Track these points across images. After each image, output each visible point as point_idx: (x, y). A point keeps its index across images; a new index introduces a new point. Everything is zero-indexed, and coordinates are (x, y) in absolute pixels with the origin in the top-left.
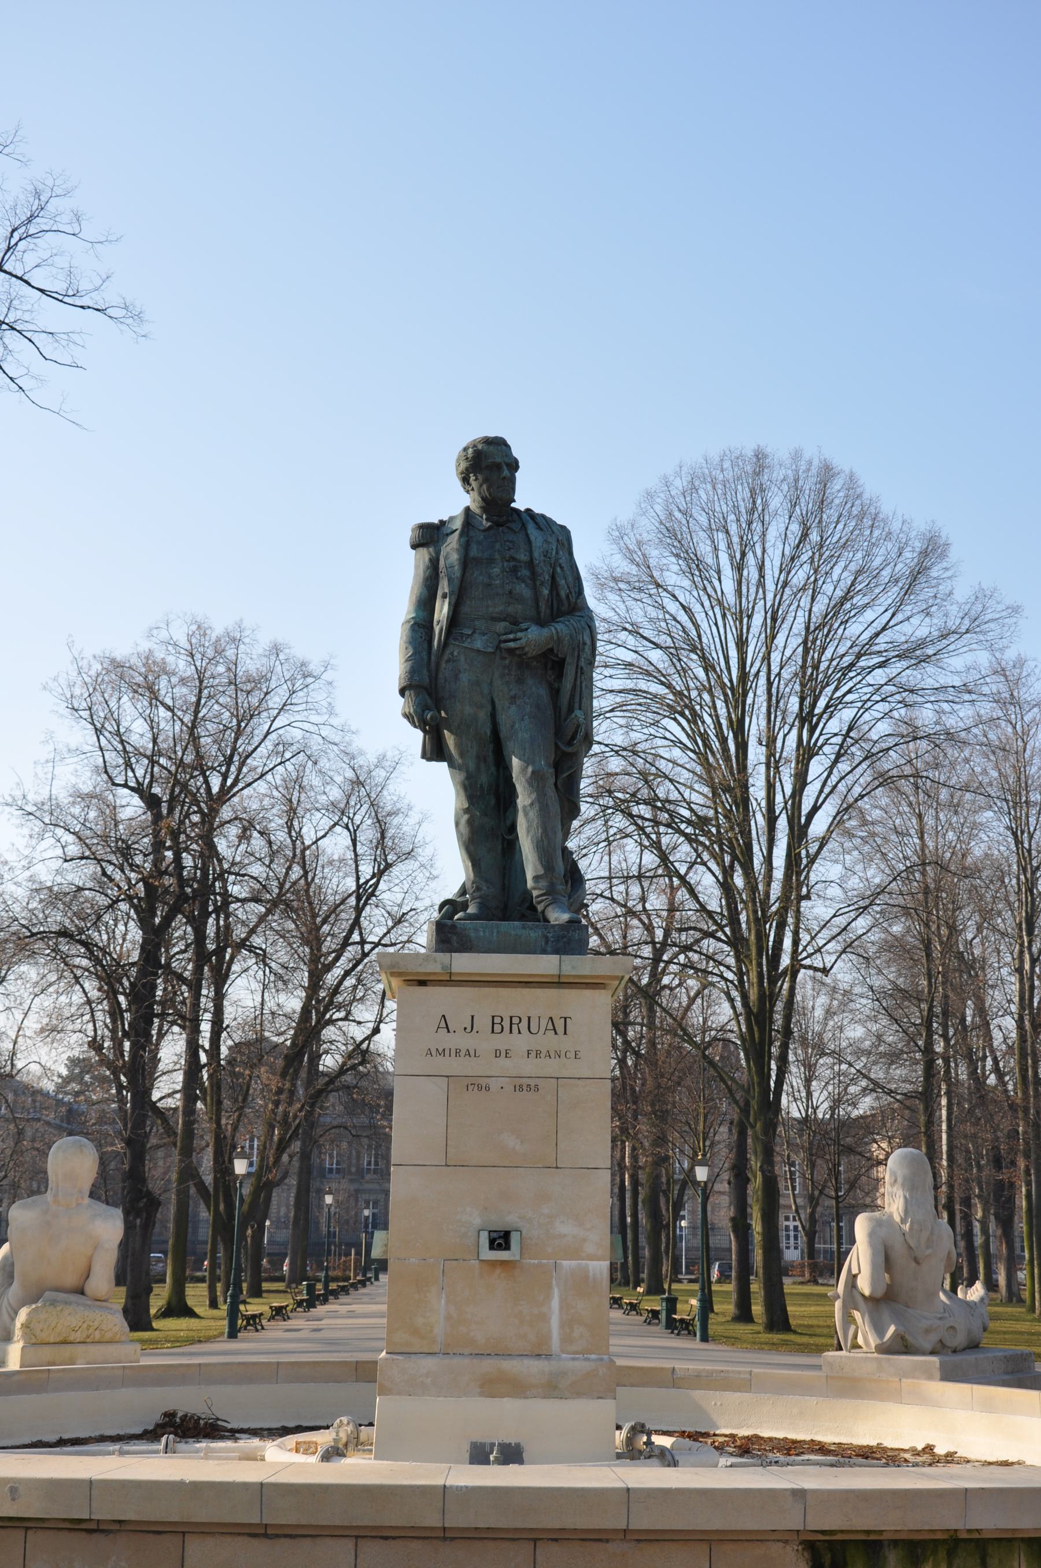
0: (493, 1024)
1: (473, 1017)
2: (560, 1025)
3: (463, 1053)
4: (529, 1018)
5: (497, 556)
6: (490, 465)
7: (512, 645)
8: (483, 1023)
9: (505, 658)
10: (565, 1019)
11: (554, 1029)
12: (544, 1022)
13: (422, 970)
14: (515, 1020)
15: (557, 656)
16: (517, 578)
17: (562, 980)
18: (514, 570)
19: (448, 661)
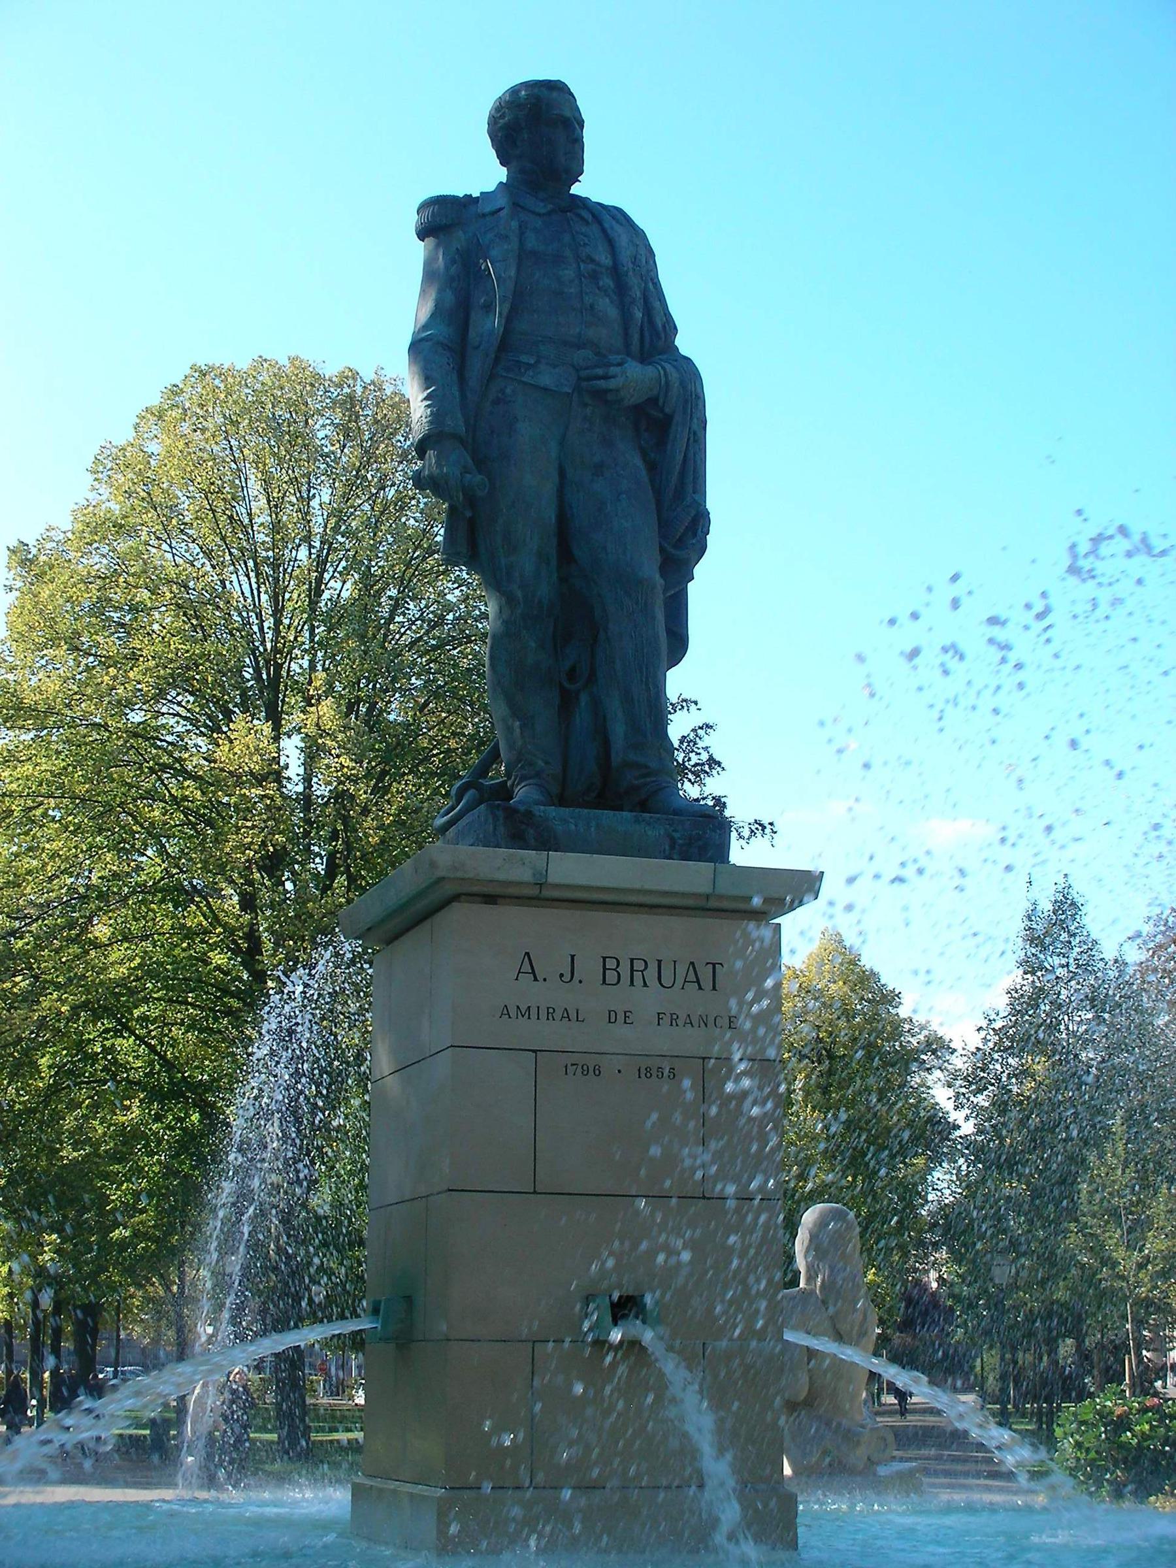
0: (605, 969)
1: (573, 957)
2: (706, 974)
3: (558, 1014)
4: (660, 962)
5: (568, 253)
6: (539, 128)
7: (602, 384)
8: (589, 967)
9: (586, 405)
10: (714, 965)
11: (698, 982)
12: (681, 970)
13: (501, 876)
14: (639, 965)
15: (662, 411)
16: (599, 288)
17: (547, 893)
18: (594, 276)
19: (497, 402)
